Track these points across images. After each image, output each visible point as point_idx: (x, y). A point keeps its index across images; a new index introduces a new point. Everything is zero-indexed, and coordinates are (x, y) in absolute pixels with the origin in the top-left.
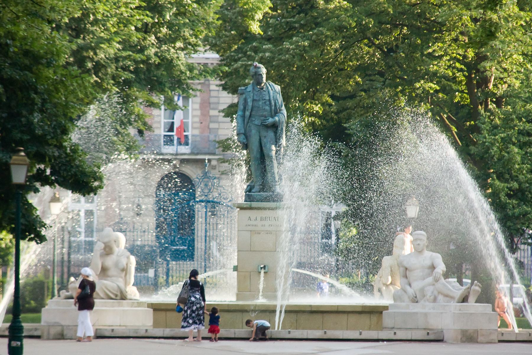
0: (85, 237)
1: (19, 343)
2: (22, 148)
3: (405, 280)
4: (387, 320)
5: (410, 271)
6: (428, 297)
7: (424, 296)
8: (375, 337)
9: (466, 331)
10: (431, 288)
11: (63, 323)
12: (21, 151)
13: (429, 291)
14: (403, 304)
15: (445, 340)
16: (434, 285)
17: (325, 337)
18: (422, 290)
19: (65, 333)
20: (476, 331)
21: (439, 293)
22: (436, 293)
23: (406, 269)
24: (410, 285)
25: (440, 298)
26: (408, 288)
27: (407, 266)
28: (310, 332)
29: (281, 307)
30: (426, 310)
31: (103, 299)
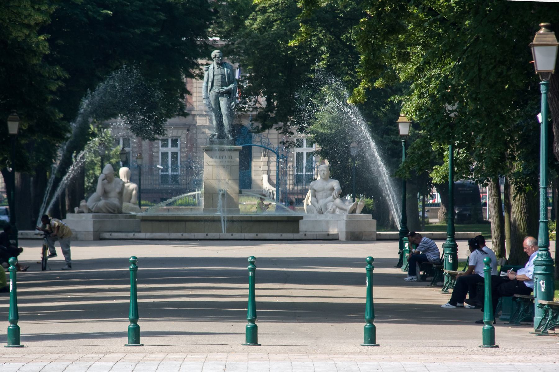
0: (306, 171)
1: (15, 241)
2: (15, 110)
3: (314, 199)
4: (303, 226)
5: (318, 192)
6: (329, 210)
7: (327, 209)
8: (291, 238)
9: (354, 232)
10: (332, 203)
11: (76, 230)
12: (14, 112)
13: (330, 206)
14: (313, 215)
15: (340, 239)
16: (333, 201)
17: (257, 238)
18: (326, 206)
19: (78, 236)
20: (361, 233)
21: (337, 207)
22: (334, 207)
23: (315, 191)
24: (317, 202)
25: (337, 210)
26: (316, 204)
27: (316, 188)
28: (246, 234)
29: (224, 217)
30: (328, 219)
31: (104, 213)
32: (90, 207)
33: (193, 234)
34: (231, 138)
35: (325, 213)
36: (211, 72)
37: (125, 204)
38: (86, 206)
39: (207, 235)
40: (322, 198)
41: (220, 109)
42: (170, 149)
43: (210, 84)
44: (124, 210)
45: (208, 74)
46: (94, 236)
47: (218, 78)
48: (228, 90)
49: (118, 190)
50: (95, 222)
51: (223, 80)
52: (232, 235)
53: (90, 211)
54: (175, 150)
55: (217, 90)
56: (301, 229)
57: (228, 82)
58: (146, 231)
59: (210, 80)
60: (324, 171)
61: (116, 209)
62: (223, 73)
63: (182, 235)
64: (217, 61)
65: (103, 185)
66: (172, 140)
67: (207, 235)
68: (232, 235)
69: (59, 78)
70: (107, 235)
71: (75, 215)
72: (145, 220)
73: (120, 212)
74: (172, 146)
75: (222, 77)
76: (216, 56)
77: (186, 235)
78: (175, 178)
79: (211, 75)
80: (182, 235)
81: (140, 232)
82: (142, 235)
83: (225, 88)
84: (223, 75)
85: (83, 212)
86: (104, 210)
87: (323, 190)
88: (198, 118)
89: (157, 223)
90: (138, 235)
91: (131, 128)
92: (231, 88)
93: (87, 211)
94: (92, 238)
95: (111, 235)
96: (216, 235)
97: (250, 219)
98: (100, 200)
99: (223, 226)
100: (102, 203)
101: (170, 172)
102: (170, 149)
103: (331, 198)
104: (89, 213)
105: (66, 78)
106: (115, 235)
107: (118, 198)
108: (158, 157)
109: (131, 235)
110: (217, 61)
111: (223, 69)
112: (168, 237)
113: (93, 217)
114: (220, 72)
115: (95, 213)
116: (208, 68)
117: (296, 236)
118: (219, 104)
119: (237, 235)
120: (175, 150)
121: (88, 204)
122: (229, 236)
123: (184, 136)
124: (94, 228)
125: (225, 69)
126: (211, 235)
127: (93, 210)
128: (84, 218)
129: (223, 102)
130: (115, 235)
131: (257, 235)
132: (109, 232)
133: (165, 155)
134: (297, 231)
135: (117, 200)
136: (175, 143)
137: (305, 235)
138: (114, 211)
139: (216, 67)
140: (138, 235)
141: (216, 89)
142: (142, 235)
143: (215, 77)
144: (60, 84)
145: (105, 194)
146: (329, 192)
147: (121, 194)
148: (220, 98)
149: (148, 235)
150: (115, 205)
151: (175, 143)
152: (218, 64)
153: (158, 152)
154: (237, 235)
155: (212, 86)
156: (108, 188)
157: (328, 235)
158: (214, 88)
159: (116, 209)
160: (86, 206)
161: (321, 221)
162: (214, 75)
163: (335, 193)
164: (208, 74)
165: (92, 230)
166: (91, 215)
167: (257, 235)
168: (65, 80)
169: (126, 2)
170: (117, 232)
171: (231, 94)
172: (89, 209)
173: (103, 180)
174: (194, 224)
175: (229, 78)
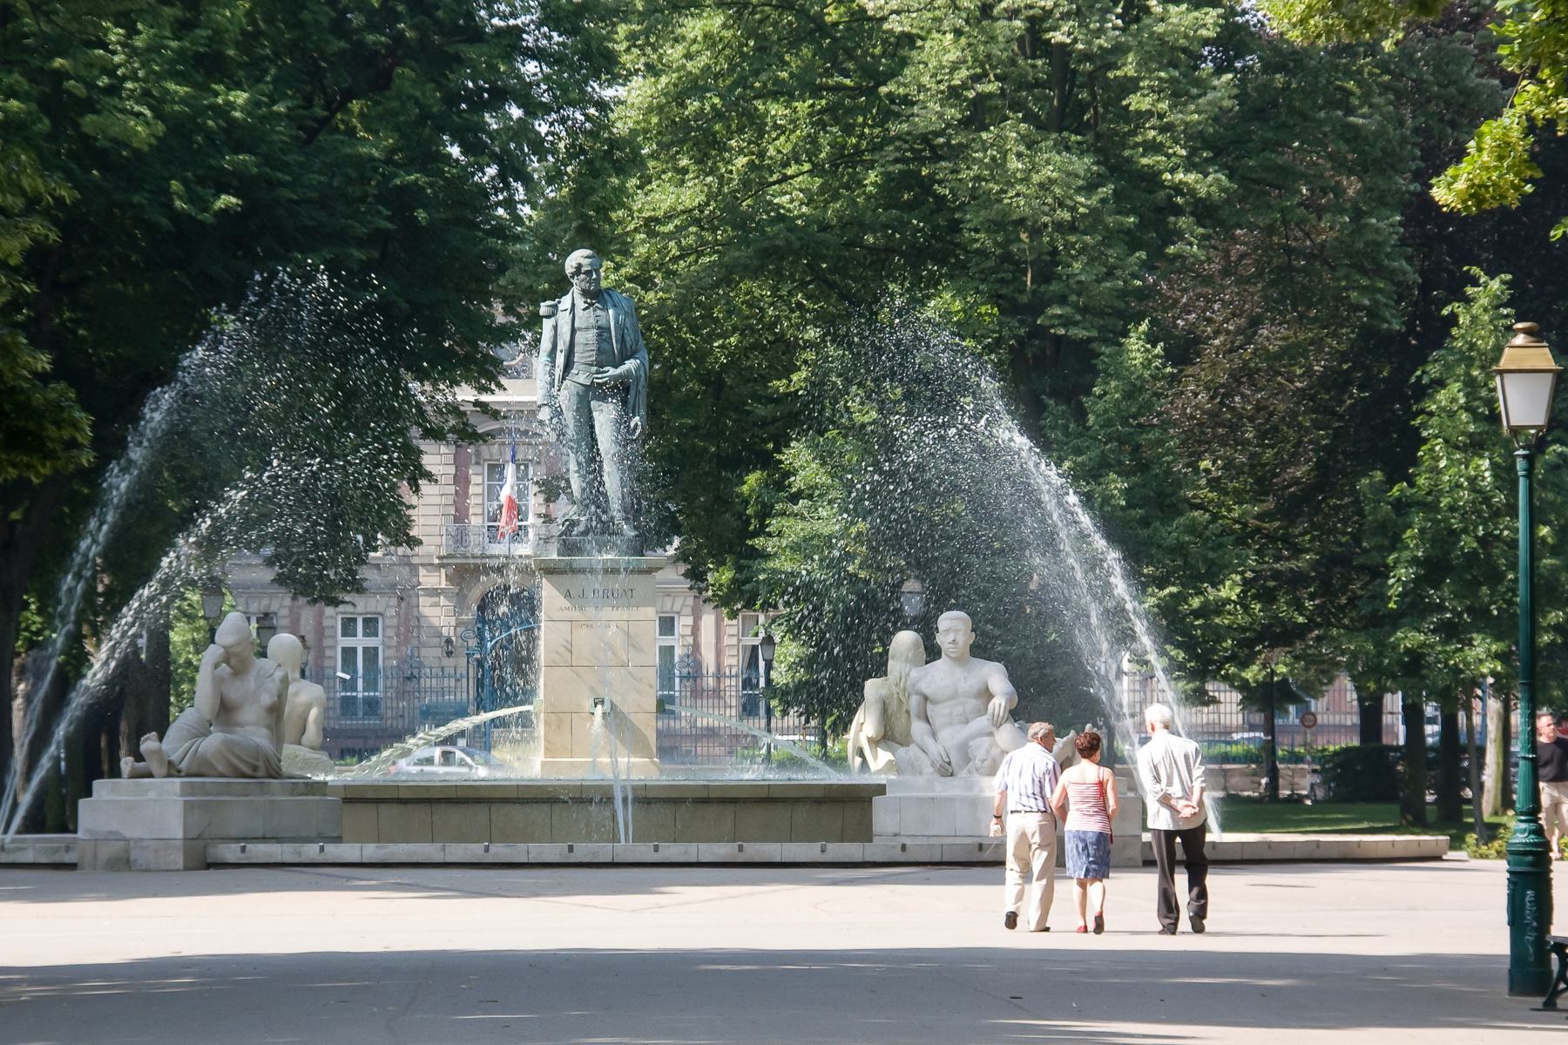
4: (883, 817)
5: (935, 703)
7: (967, 759)
11: (128, 835)
14: (921, 780)
23: (926, 698)
24: (934, 735)
27: (927, 691)
31: (223, 776)
32: (174, 757)
33: (522, 847)
34: (629, 532)
35: (963, 774)
36: (564, 319)
37: (289, 749)
38: (159, 752)
39: (571, 849)
40: (950, 724)
41: (594, 440)
42: (360, 642)
43: (560, 359)
44: (285, 767)
45: (555, 328)
46: (187, 852)
47: (587, 338)
48: (620, 376)
49: (266, 699)
50: (189, 807)
51: (605, 345)
52: (656, 849)
53: (172, 770)
54: (371, 642)
55: (583, 379)
56: (876, 828)
57: (621, 352)
58: (360, 838)
59: (561, 346)
60: (956, 631)
61: (261, 764)
62: (602, 322)
63: (487, 850)
64: (585, 285)
65: (218, 682)
66: (365, 620)
67: (571, 849)
68: (656, 849)
69: (33, 204)
70: (230, 852)
71: (124, 782)
72: (356, 798)
73: (275, 773)
74: (365, 635)
75: (599, 335)
76: (579, 266)
77: (500, 851)
78: (372, 705)
79: (565, 330)
80: (487, 850)
81: (338, 839)
82: (347, 851)
83: (612, 371)
84: (603, 331)
85: (150, 775)
86: (220, 768)
87: (954, 696)
88: (422, 571)
89: (395, 809)
90: (335, 851)
91: (280, 580)
92: (629, 371)
93: (164, 771)
94: (180, 866)
95: (243, 849)
96: (604, 851)
97: (704, 795)
98: (206, 734)
99: (624, 816)
100: (213, 742)
101: (360, 694)
102: (360, 642)
103: (982, 722)
104: (169, 776)
105: (59, 201)
106: (260, 851)
107: (268, 727)
108: (335, 658)
109: (311, 851)
110: (585, 285)
111: (605, 309)
112: (439, 858)
113: (187, 790)
114: (592, 321)
115: (188, 776)
116: (555, 307)
117: (852, 851)
118: (591, 418)
119: (673, 851)
120: (371, 642)
121: (166, 744)
122: (644, 852)
123: (392, 612)
124: (185, 832)
125: (611, 311)
126: (583, 851)
127: (183, 766)
128: (152, 795)
129: (605, 416)
130: (260, 851)
131: (741, 848)
132: (238, 840)
133: (349, 653)
134: (864, 833)
135: (264, 731)
136: (371, 625)
137: (904, 847)
138: (255, 768)
139: (580, 303)
140: (335, 851)
141: (581, 376)
142: (347, 851)
143: (579, 337)
144: (38, 227)
145: (225, 711)
146: (972, 704)
147: (276, 711)
148: (594, 404)
149: (371, 851)
150: (258, 748)
151: (371, 625)
152: (585, 293)
153: (334, 647)
154: (673, 851)
155: (568, 365)
156: (234, 692)
157: (981, 846)
158: (574, 371)
159: (261, 764)
160: (159, 752)
161: (950, 800)
162: (573, 331)
163: (999, 703)
164: (555, 328)
165: (181, 836)
166: (178, 780)
167: (741, 848)
168: (59, 214)
169: (280, 175)
170: (264, 839)
171: (627, 390)
172: (170, 763)
173: (216, 666)
174: (538, 814)
175: (622, 341)
